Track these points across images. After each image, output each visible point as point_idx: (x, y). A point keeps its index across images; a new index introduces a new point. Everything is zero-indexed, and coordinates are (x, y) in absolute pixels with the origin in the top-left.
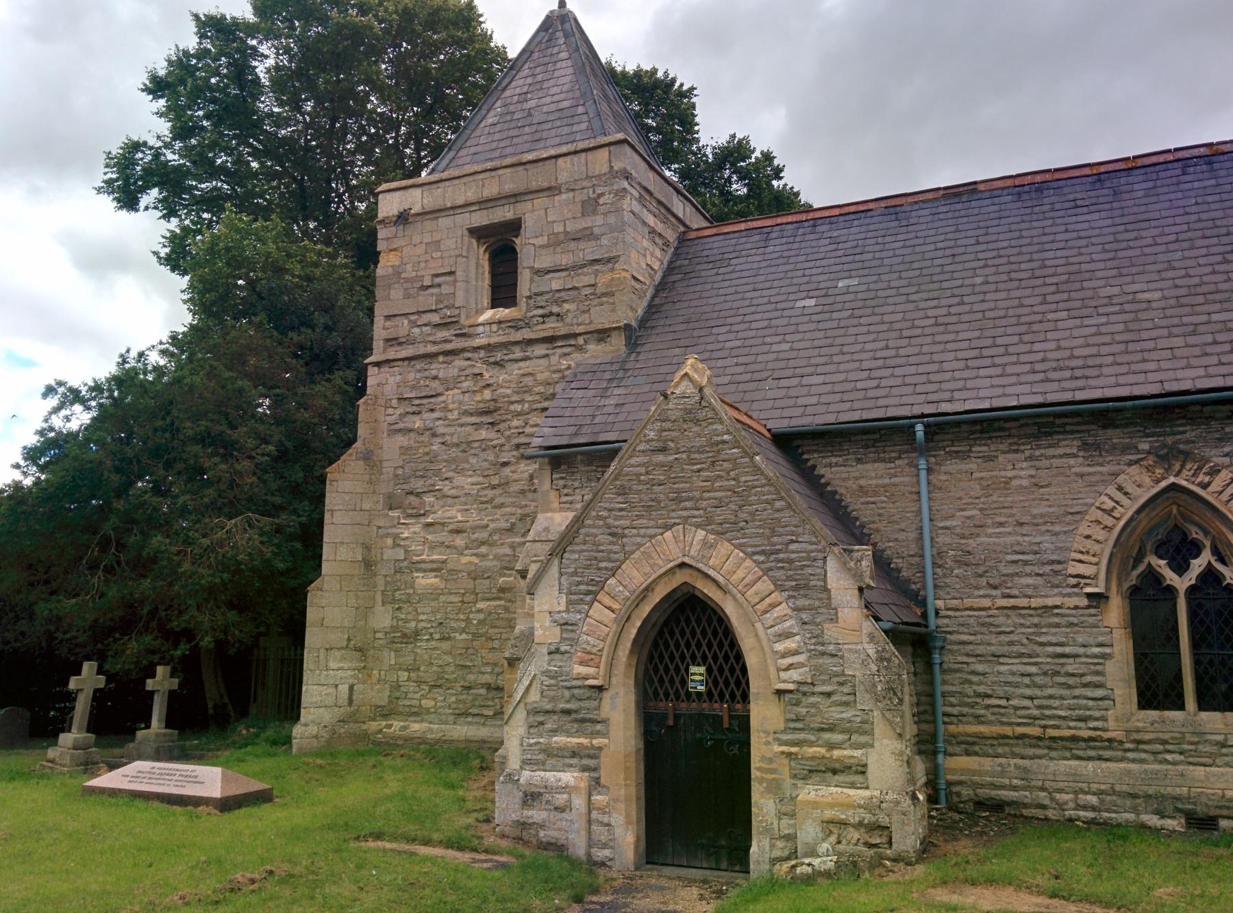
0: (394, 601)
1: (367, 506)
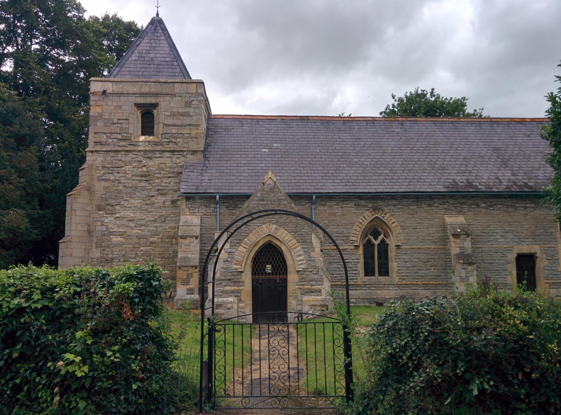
0: (101, 247)
1: (89, 209)
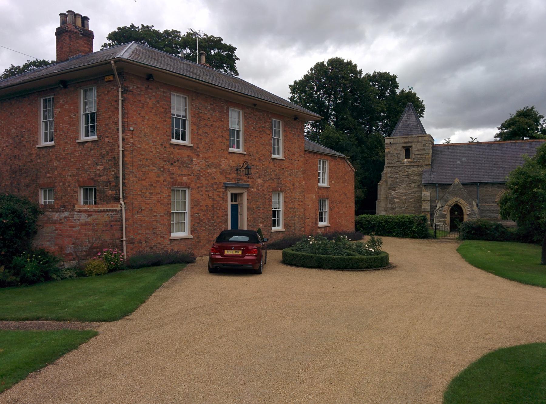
0: (391, 203)
